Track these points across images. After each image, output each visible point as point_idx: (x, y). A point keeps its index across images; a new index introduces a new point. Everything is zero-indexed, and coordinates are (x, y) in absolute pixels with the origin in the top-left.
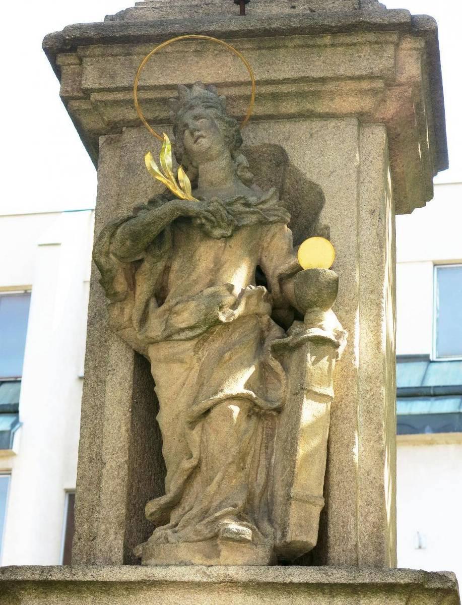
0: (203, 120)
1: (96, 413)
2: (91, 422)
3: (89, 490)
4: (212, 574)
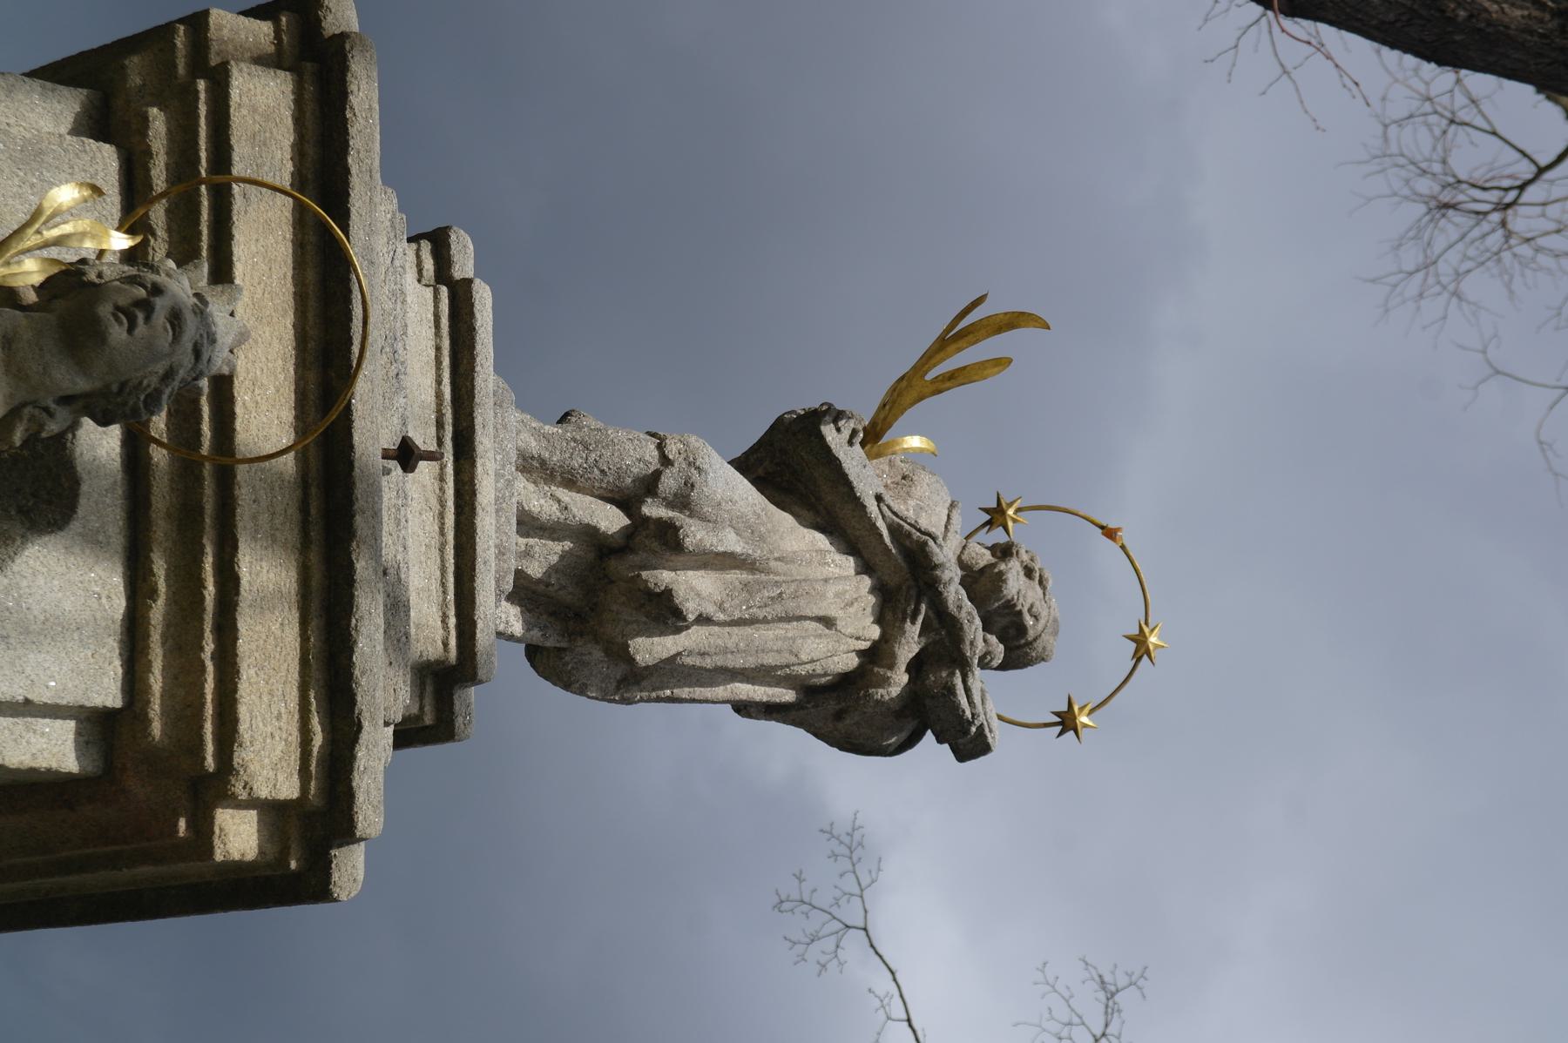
0: (171, 333)
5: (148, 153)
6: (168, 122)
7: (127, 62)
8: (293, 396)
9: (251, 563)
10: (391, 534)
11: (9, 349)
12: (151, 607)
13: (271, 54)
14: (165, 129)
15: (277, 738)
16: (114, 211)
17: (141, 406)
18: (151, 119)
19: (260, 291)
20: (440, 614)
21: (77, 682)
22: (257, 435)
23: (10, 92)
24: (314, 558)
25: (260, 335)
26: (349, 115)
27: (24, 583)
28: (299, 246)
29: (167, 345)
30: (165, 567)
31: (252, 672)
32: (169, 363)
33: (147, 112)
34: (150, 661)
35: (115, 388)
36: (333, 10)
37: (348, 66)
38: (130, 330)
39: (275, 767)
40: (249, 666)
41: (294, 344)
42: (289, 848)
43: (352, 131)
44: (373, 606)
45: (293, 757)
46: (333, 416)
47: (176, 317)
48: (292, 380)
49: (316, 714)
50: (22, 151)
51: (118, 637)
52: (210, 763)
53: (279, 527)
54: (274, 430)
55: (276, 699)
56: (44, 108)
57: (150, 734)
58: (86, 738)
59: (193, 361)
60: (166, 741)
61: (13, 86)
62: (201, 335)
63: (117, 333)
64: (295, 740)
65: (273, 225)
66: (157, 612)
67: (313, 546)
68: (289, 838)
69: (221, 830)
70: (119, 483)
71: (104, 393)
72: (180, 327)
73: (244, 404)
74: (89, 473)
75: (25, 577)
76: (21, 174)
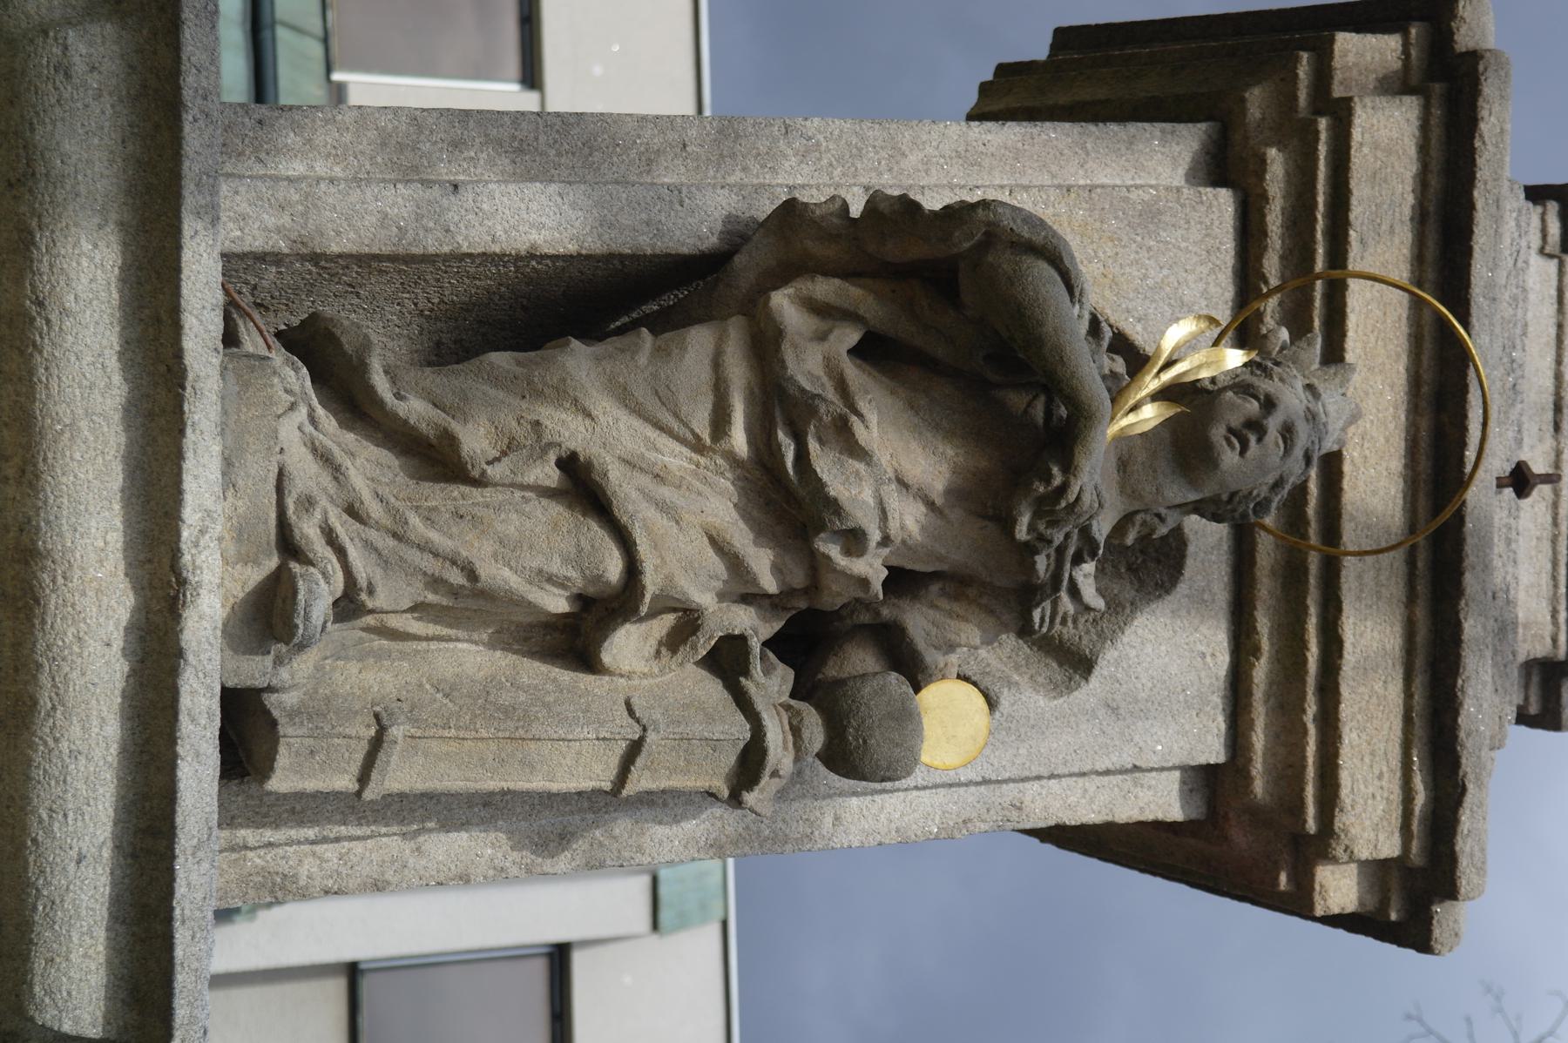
0: (1282, 449)
1: (573, 154)
2: (551, 142)
3: (384, 144)
4: (200, 553)
5: (1264, 197)
6: (1286, 162)
7: (1247, 95)
8: (1403, 444)
9: (1355, 624)
10: (1500, 556)
11: (1125, 472)
12: (1254, 665)
13: (1397, 72)
14: (1283, 171)
15: (1379, 798)
16: (1228, 258)
17: (1251, 512)
18: (1269, 161)
19: (1373, 339)
20: (1550, 608)
21: (1182, 743)
22: (1365, 491)
23: (1131, 143)
24: (1421, 613)
25: (1371, 386)
26: (1477, 144)
27: (1133, 653)
28: (1416, 340)
29: (1278, 460)
30: (1269, 624)
31: (1354, 735)
32: (1279, 473)
33: (1265, 154)
34: (1253, 720)
35: (1225, 497)
36: (1468, 21)
37: (1480, 91)
38: (1242, 453)
39: (1376, 828)
40: (1351, 730)
41: (1406, 389)
42: (1389, 899)
43: (1480, 161)
44: (1481, 664)
45: (1394, 815)
46: (1447, 514)
47: (1288, 432)
48: (1403, 427)
49: (1418, 772)
50: (1140, 215)
51: (1221, 693)
52: (1311, 826)
53: (1385, 582)
54: (1382, 483)
55: (1377, 759)
56: (1163, 154)
57: (1252, 792)
58: (1190, 786)
59: (1303, 467)
60: (1268, 798)
61: (1134, 136)
62: (1313, 442)
63: (1229, 458)
64: (1396, 799)
65: (1390, 267)
66: (1261, 671)
67: (1419, 601)
68: (1389, 890)
69: (1321, 886)
70: (1225, 539)
71: (1215, 500)
72: (1292, 441)
73: (1352, 461)
74: (1196, 533)
75: (1134, 647)
76: (1139, 239)
